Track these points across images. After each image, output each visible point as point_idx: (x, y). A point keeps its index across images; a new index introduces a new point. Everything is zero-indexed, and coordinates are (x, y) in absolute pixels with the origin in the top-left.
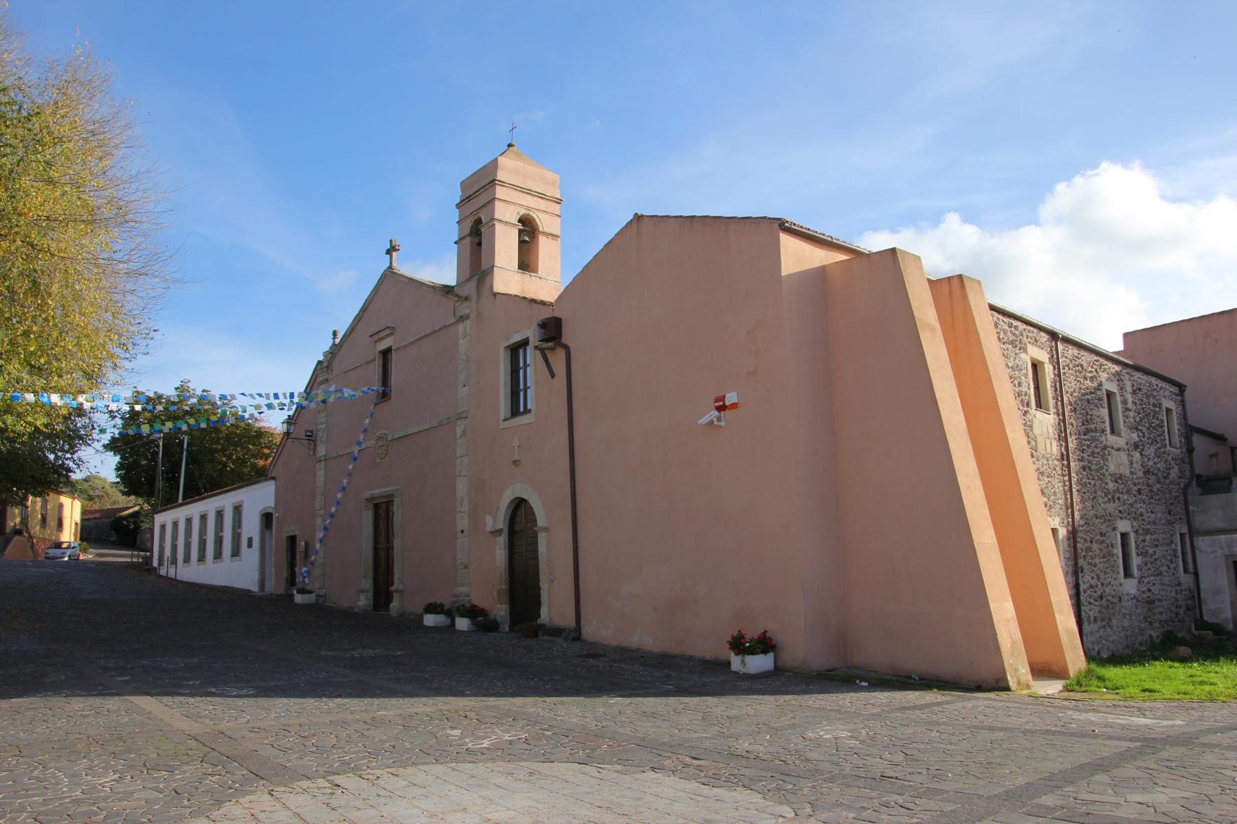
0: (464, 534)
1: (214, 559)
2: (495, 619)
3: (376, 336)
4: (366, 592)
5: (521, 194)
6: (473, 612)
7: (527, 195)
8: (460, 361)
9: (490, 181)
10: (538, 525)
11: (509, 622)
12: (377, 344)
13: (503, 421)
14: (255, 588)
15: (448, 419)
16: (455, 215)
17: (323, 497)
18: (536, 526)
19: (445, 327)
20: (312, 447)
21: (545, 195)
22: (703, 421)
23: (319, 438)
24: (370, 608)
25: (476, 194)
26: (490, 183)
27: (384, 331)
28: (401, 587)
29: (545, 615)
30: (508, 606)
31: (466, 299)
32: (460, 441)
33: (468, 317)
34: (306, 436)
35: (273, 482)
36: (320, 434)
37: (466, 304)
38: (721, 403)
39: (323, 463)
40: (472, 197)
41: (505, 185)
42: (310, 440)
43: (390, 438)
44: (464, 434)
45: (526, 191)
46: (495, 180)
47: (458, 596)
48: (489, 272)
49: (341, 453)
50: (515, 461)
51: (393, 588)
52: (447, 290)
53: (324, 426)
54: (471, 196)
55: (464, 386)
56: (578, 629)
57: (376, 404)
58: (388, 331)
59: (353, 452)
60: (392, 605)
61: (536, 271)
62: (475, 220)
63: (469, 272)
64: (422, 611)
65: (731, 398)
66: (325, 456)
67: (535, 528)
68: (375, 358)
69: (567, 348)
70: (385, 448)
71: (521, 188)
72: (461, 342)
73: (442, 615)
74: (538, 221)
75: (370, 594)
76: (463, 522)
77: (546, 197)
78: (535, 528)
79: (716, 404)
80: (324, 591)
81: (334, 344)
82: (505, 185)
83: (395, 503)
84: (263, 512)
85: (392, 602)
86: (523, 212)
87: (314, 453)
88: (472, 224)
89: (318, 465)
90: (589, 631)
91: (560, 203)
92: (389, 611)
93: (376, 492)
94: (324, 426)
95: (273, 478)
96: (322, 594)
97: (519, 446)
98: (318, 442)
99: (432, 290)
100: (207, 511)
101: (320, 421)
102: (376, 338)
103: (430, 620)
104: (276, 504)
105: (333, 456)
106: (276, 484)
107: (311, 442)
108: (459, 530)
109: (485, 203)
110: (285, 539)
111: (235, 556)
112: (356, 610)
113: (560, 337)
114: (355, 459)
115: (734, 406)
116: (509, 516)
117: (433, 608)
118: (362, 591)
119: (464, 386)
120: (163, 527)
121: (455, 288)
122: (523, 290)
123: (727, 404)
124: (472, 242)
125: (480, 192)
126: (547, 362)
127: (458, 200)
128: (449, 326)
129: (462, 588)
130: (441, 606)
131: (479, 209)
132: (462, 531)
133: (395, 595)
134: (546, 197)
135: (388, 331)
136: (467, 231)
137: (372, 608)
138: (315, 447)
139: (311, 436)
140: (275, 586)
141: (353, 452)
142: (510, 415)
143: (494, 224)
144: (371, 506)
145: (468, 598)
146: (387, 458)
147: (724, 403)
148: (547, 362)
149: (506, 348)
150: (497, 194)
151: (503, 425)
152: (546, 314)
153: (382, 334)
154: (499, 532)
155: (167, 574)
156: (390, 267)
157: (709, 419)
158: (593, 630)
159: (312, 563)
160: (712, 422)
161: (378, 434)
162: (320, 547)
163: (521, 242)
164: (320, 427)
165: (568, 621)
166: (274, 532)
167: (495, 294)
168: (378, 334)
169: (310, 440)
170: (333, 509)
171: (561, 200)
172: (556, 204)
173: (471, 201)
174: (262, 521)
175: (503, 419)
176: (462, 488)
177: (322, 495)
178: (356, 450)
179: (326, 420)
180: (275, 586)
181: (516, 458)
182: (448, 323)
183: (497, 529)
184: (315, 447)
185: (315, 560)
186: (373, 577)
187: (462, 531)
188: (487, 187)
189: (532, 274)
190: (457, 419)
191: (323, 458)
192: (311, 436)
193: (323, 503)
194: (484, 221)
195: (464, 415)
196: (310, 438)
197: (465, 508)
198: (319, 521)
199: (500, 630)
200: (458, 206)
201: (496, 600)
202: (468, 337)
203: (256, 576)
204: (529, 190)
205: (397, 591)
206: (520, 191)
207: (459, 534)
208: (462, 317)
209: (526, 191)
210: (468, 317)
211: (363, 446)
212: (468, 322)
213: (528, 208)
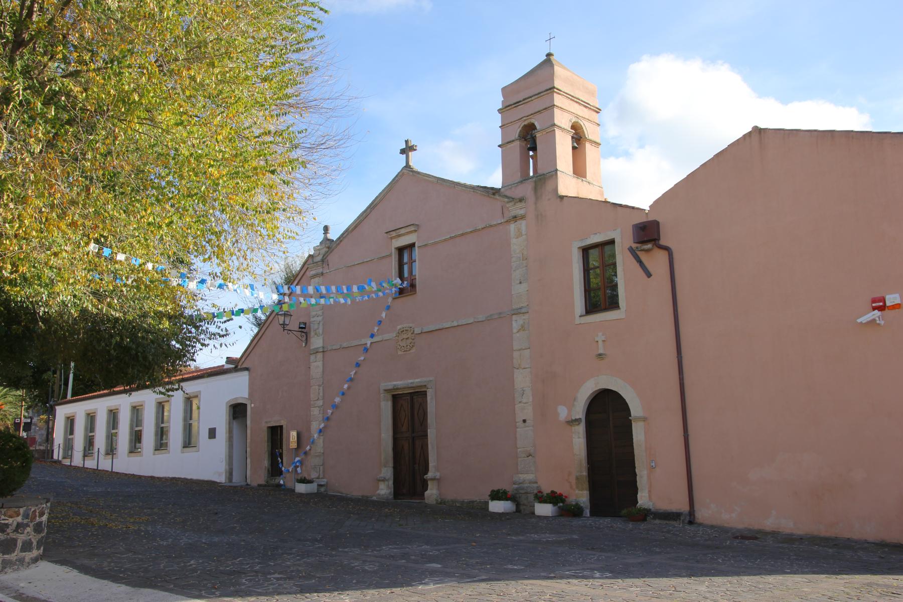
0: (527, 424)
1: (155, 450)
2: (577, 504)
3: (394, 233)
4: (387, 480)
5: (571, 102)
6: (554, 498)
7: (575, 103)
8: (514, 259)
9: (548, 88)
10: (632, 415)
11: (589, 507)
12: (393, 240)
13: (580, 316)
14: (221, 479)
15: (500, 314)
16: (498, 120)
17: (321, 388)
18: (631, 416)
19: (491, 226)
20: (304, 339)
21: (589, 104)
22: (864, 319)
23: (312, 330)
24: (391, 497)
25: (526, 101)
26: (547, 90)
27: (407, 228)
28: (438, 475)
29: (643, 499)
30: (588, 492)
31: (521, 200)
32: (518, 335)
33: (523, 217)
34: (300, 328)
35: (246, 373)
36: (314, 327)
37: (519, 205)
38: (881, 304)
39: (320, 355)
40: (520, 103)
41: (562, 93)
42: (303, 332)
43: (417, 331)
44: (523, 328)
45: (575, 99)
46: (554, 88)
47: (521, 483)
48: (552, 176)
49: (345, 345)
50: (357, 363)
51: (430, 475)
52: (494, 191)
53: (320, 318)
54: (520, 101)
55: (520, 283)
56: (692, 513)
57: (394, 299)
58: (412, 228)
59: (366, 344)
60: (427, 493)
61: (585, 177)
62: (525, 126)
63: (519, 174)
64: (487, 498)
65: (892, 299)
66: (323, 347)
67: (630, 418)
68: (392, 253)
69: (666, 249)
70: (410, 341)
71: (573, 97)
72: (514, 241)
73: (509, 502)
74: (584, 128)
75: (391, 482)
76: (525, 410)
77: (589, 106)
78: (630, 418)
79: (874, 305)
80: (325, 480)
81: (326, 240)
82: (562, 93)
83: (428, 394)
84: (232, 403)
85: (427, 489)
86: (574, 120)
87: (306, 345)
88: (520, 129)
89: (312, 357)
90: (704, 514)
91: (598, 113)
92: (424, 499)
93: (399, 383)
94: (320, 318)
95: (247, 369)
96: (322, 483)
97: (604, 341)
98: (312, 334)
99: (472, 190)
100: (144, 402)
101: (313, 313)
102: (394, 234)
103: (497, 507)
104: (251, 394)
105: (334, 347)
106: (250, 375)
107: (303, 334)
108: (519, 419)
109: (542, 108)
110: (266, 429)
111: (187, 447)
112: (375, 498)
113: (659, 239)
114: (366, 350)
115: (896, 307)
116: (587, 406)
117: (497, 495)
118: (384, 480)
119: (520, 283)
120: (70, 422)
121: (501, 190)
122: (578, 194)
123: (888, 304)
124: (521, 146)
125: (533, 98)
126: (640, 262)
127: (500, 107)
128: (495, 225)
129: (526, 475)
130: (505, 492)
131: (532, 114)
132: (524, 421)
133: (429, 483)
134: (589, 106)
135: (412, 228)
136: (516, 134)
137: (392, 496)
138: (307, 339)
139: (304, 328)
140: (257, 476)
141: (366, 344)
142: (584, 313)
143: (555, 130)
144: (389, 397)
145: (535, 485)
146: (413, 351)
147: (885, 303)
148: (640, 262)
149: (579, 248)
150: (555, 102)
151: (578, 320)
152: (643, 219)
153: (402, 231)
154: (578, 421)
155: (98, 467)
156: (407, 166)
157: (872, 318)
158: (706, 513)
159: (306, 453)
160: (874, 320)
161: (399, 327)
162: (318, 438)
163: (574, 148)
164: (312, 319)
165: (680, 504)
166: (249, 422)
167: (562, 197)
168: (398, 231)
169: (303, 332)
170: (337, 400)
171: (600, 110)
172: (595, 113)
173: (518, 107)
174: (228, 409)
175: (579, 314)
176: (522, 380)
177: (319, 386)
178: (369, 342)
179: (323, 313)
180: (257, 476)
181: (601, 351)
182: (495, 223)
183: (574, 418)
184: (307, 339)
185: (310, 450)
186: (393, 466)
187: (524, 421)
188: (542, 94)
189: (584, 179)
190: (513, 314)
191: (321, 350)
192: (304, 328)
193: (321, 394)
194: (538, 127)
195: (523, 310)
196: (303, 330)
197: (528, 397)
198: (315, 412)
199: (584, 515)
200: (500, 111)
201: (574, 487)
202: (524, 236)
203: (222, 467)
204: (578, 99)
205: (432, 479)
206: (571, 100)
207: (520, 424)
208: (515, 217)
209: (575, 99)
210: (523, 217)
211: (375, 339)
212: (523, 224)
213: (577, 116)
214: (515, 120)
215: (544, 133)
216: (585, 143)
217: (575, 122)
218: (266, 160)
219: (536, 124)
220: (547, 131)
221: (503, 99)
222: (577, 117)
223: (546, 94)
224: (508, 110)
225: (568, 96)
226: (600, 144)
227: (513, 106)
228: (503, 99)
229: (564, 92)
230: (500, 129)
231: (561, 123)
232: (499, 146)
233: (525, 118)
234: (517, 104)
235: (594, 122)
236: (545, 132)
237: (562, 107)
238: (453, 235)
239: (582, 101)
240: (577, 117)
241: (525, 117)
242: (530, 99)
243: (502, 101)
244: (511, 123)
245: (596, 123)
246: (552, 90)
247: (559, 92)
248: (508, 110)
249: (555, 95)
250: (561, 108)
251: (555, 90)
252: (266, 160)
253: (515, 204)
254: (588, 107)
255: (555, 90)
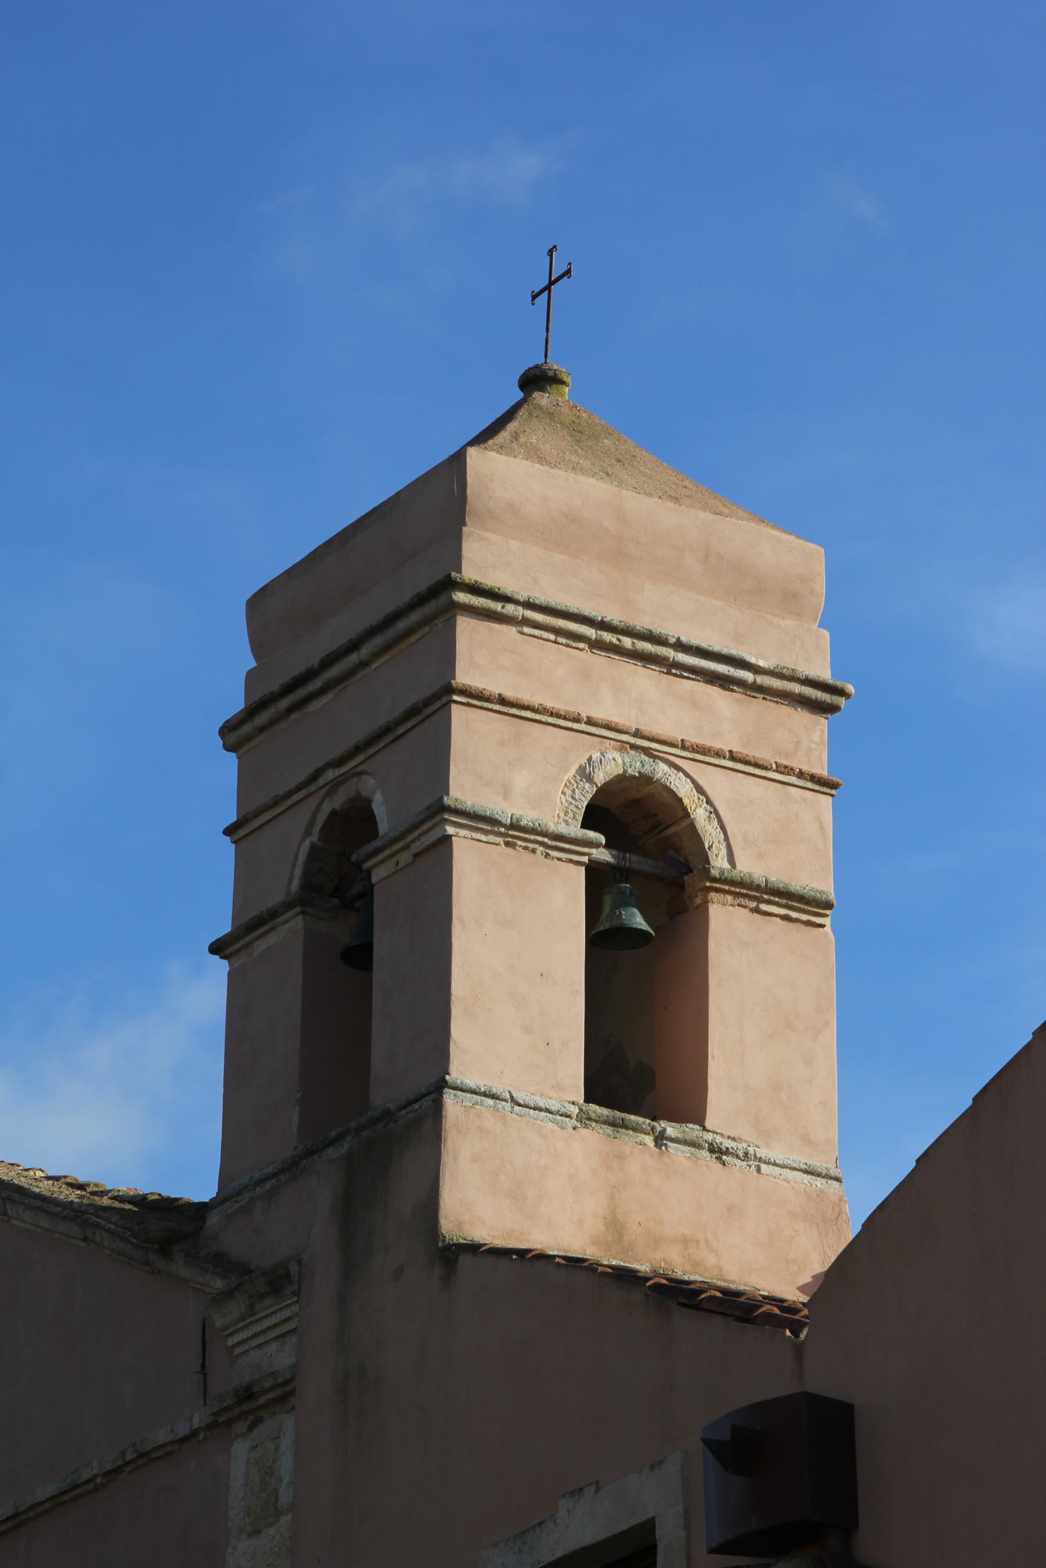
5: (599, 661)
9: (422, 586)
19: (146, 1458)
40: (316, 684)
41: (510, 609)
71: (603, 625)
74: (700, 814)
82: (510, 609)
121: (213, 1220)
122: (615, 1225)
125: (364, 652)
131: (357, 749)
171: (840, 692)
182: (162, 1436)
188: (401, 625)
189: (672, 1130)
209: (627, 642)
214: (292, 785)
215: (405, 858)
216: (706, 903)
217: (621, 781)
218: (798, 743)
219: (379, 808)
220: (417, 847)
221: (252, 663)
222: (646, 751)
223: (421, 624)
224: (262, 729)
225: (561, 623)
226: (829, 905)
227: (284, 703)
228: (252, 663)
229: (529, 605)
230: (228, 847)
231: (506, 791)
232: (217, 948)
233: (331, 774)
234: (301, 693)
235: (787, 770)
236: (405, 858)
237: (509, 694)
238: (51, 1490)
239: (680, 646)
240: (646, 751)
241: (328, 766)
242: (353, 658)
243: (249, 674)
244: (275, 803)
245: (801, 775)
246: (442, 600)
247: (497, 606)
248: (262, 729)
249: (465, 627)
250: (502, 701)
251: (461, 597)
252: (798, 743)
253: (251, 1310)
254: (741, 683)
255: (461, 597)
